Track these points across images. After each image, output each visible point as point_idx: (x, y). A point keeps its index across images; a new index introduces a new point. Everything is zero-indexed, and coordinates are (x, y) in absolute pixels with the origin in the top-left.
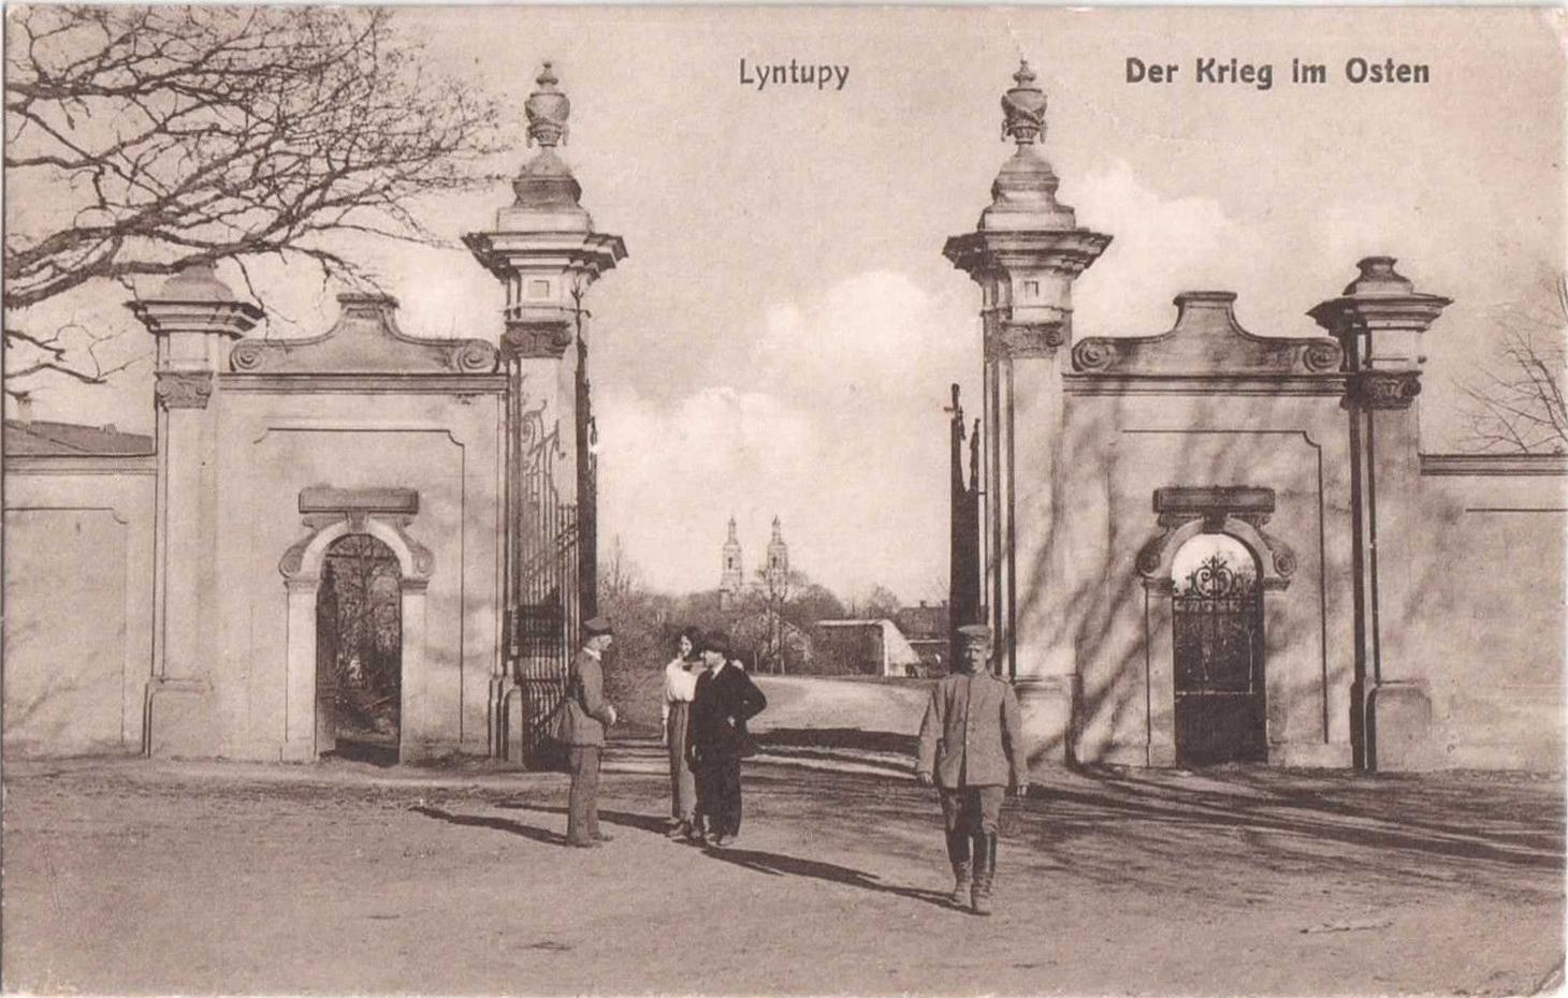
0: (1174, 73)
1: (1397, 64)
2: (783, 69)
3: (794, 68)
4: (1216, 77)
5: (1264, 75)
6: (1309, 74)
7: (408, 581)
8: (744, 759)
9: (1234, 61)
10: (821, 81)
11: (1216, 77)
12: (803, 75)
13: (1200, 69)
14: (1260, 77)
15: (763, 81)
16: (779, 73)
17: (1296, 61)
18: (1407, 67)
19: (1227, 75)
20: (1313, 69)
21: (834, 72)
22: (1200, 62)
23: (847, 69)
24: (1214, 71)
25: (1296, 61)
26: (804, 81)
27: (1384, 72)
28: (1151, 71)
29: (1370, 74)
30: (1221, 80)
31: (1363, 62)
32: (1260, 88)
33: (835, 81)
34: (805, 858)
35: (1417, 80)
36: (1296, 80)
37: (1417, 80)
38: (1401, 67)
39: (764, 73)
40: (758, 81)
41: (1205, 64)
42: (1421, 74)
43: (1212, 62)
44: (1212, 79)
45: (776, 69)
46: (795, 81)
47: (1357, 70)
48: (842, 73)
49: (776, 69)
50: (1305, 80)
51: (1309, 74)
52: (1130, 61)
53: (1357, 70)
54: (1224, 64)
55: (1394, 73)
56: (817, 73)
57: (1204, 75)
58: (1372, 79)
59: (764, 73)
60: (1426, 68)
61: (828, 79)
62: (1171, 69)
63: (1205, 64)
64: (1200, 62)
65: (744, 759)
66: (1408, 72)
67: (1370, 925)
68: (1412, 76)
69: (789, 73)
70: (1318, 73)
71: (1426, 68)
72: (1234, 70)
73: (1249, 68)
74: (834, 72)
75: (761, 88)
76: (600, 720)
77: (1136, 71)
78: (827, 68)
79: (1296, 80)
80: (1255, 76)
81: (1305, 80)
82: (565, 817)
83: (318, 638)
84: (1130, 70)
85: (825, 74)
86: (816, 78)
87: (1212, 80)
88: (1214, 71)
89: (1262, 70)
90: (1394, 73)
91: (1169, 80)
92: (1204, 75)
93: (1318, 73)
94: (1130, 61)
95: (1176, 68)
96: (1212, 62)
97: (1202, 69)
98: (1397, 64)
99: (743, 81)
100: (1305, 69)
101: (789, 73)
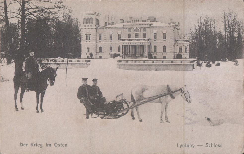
0: (27, 145)
1: (62, 144)
2: (184, 145)
3: (186, 145)
4: (34, 146)
5: (41, 145)
6: (49, 145)
7: (128, 107)
9: (36, 143)
11: (34, 146)
12: (184, 146)
14: (40, 146)
15: (181, 147)
16: (183, 146)
17: (46, 143)
18: (64, 144)
19: (35, 145)
20: (49, 144)
21: (192, 146)
22: (31, 143)
23: (31, 146)
24: (33, 145)
25: (46, 143)
26: (187, 147)
27: (60, 145)
29: (58, 145)
30: (34, 146)
31: (22, 143)
32: (41, 147)
33: (192, 147)
35: (65, 146)
37: (65, 146)
38: (63, 144)
39: (181, 145)
40: (180, 146)
41: (32, 143)
42: (66, 145)
43: (33, 143)
44: (33, 146)
45: (183, 145)
46: (61, 146)
47: (56, 145)
48: (193, 145)
49: (183, 145)
50: (49, 146)
51: (49, 145)
52: (20, 143)
53: (56, 145)
54: (35, 144)
55: (62, 145)
57: (32, 145)
58: (58, 146)
59: (181, 145)
60: (67, 144)
62: (27, 144)
63: (32, 143)
64: (31, 143)
66: (25, 145)
69: (185, 146)
70: (50, 145)
73: (63, 145)
74: (192, 146)
75: (180, 148)
77: (21, 145)
78: (191, 145)
80: (40, 146)
81: (48, 146)
82: (127, 107)
83: (15, 88)
85: (191, 146)
86: (189, 147)
88: (33, 145)
89: (41, 144)
90: (62, 145)
91: (26, 146)
92: (32, 145)
93: (50, 145)
94: (20, 143)
95: (27, 144)
96: (33, 143)
97: (32, 145)
98: (62, 144)
99: (178, 147)
100: (48, 144)
101: (185, 146)
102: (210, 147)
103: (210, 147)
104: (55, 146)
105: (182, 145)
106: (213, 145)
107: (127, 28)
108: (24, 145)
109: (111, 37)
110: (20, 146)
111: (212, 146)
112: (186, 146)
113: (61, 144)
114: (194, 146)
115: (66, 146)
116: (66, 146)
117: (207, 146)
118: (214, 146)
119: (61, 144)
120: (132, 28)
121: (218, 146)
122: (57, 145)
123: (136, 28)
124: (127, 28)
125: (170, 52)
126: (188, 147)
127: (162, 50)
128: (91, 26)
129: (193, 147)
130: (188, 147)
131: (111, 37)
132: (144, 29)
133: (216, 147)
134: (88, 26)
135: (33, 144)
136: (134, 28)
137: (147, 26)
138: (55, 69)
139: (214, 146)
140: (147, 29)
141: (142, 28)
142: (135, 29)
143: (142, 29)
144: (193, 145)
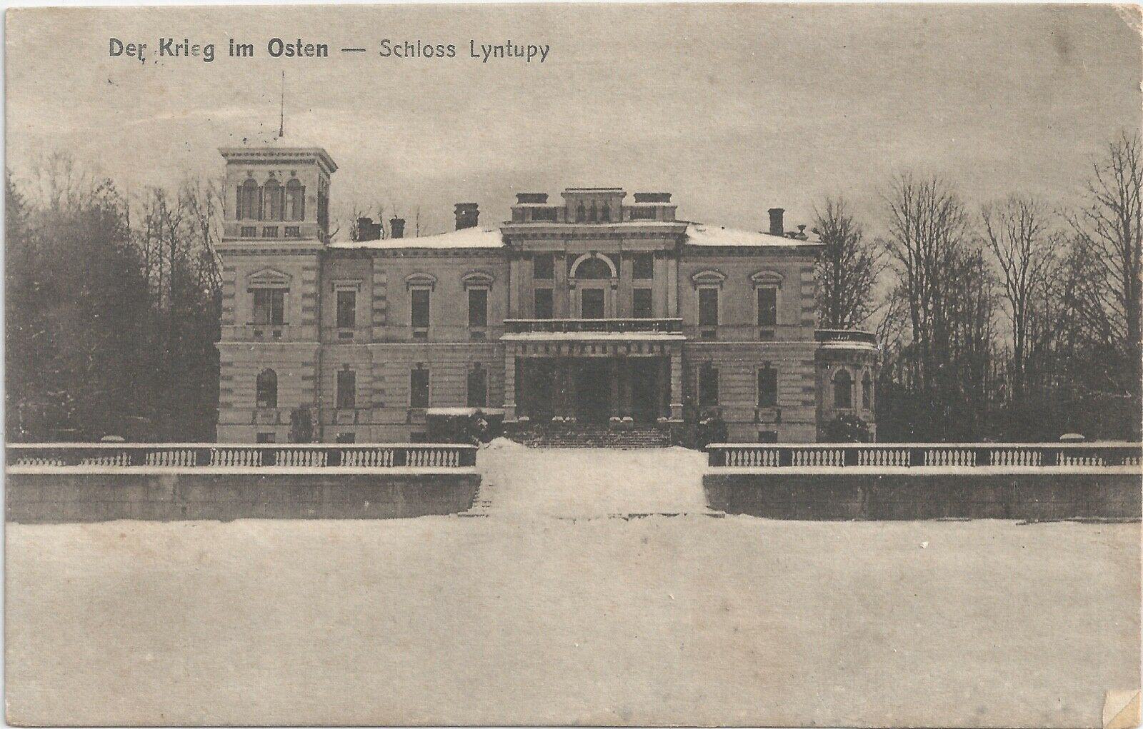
2: (501, 47)
4: (174, 53)
6: (241, 49)
8: (326, 454)
9: (186, 41)
10: (529, 56)
11: (174, 53)
12: (502, 50)
13: (162, 48)
15: (487, 56)
17: (232, 40)
20: (244, 46)
22: (162, 40)
25: (232, 40)
27: (295, 49)
28: (128, 48)
29: (285, 50)
31: (120, 43)
33: (539, 56)
34: (148, 524)
35: (319, 55)
36: (231, 55)
37: (319, 55)
39: (487, 49)
41: (166, 42)
44: (171, 54)
46: (300, 55)
47: (276, 46)
50: (238, 55)
51: (241, 49)
53: (276, 46)
55: (302, 49)
56: (526, 51)
59: (487, 49)
60: (325, 46)
61: (534, 54)
63: (166, 42)
64: (162, 40)
65: (326, 454)
67: (830, 458)
68: (315, 52)
70: (247, 49)
71: (325, 46)
72: (186, 46)
74: (539, 50)
76: (593, 401)
77: (117, 49)
79: (231, 55)
81: (238, 55)
84: (112, 49)
87: (171, 54)
88: (172, 47)
90: (512, 52)
93: (247, 49)
98: (304, 43)
100: (238, 47)
101: (505, 50)
102: (400, 56)
103: (400, 56)
104: (273, 55)
105: (493, 49)
106: (412, 47)
107: (528, 256)
108: (132, 52)
109: (420, 312)
110: (112, 54)
111: (410, 50)
112: (512, 49)
113: (299, 46)
114: (547, 52)
115: (241, 54)
116: (241, 54)
117: (386, 51)
118: (416, 54)
119: (299, 46)
120: (560, 255)
121: (436, 51)
122: (432, 54)
123: (588, 256)
124: (528, 256)
125: (505, 288)
126: (522, 55)
127: (228, 265)
128: (294, 233)
129: (544, 56)
130: (522, 55)
131: (420, 312)
132: (643, 264)
133: (424, 53)
134: (271, 232)
135: (169, 44)
136: (572, 258)
137: (660, 244)
138: (314, 257)
139: (416, 54)
140: (658, 264)
141: (626, 255)
142: (579, 261)
143: (627, 265)
144: (545, 49)
